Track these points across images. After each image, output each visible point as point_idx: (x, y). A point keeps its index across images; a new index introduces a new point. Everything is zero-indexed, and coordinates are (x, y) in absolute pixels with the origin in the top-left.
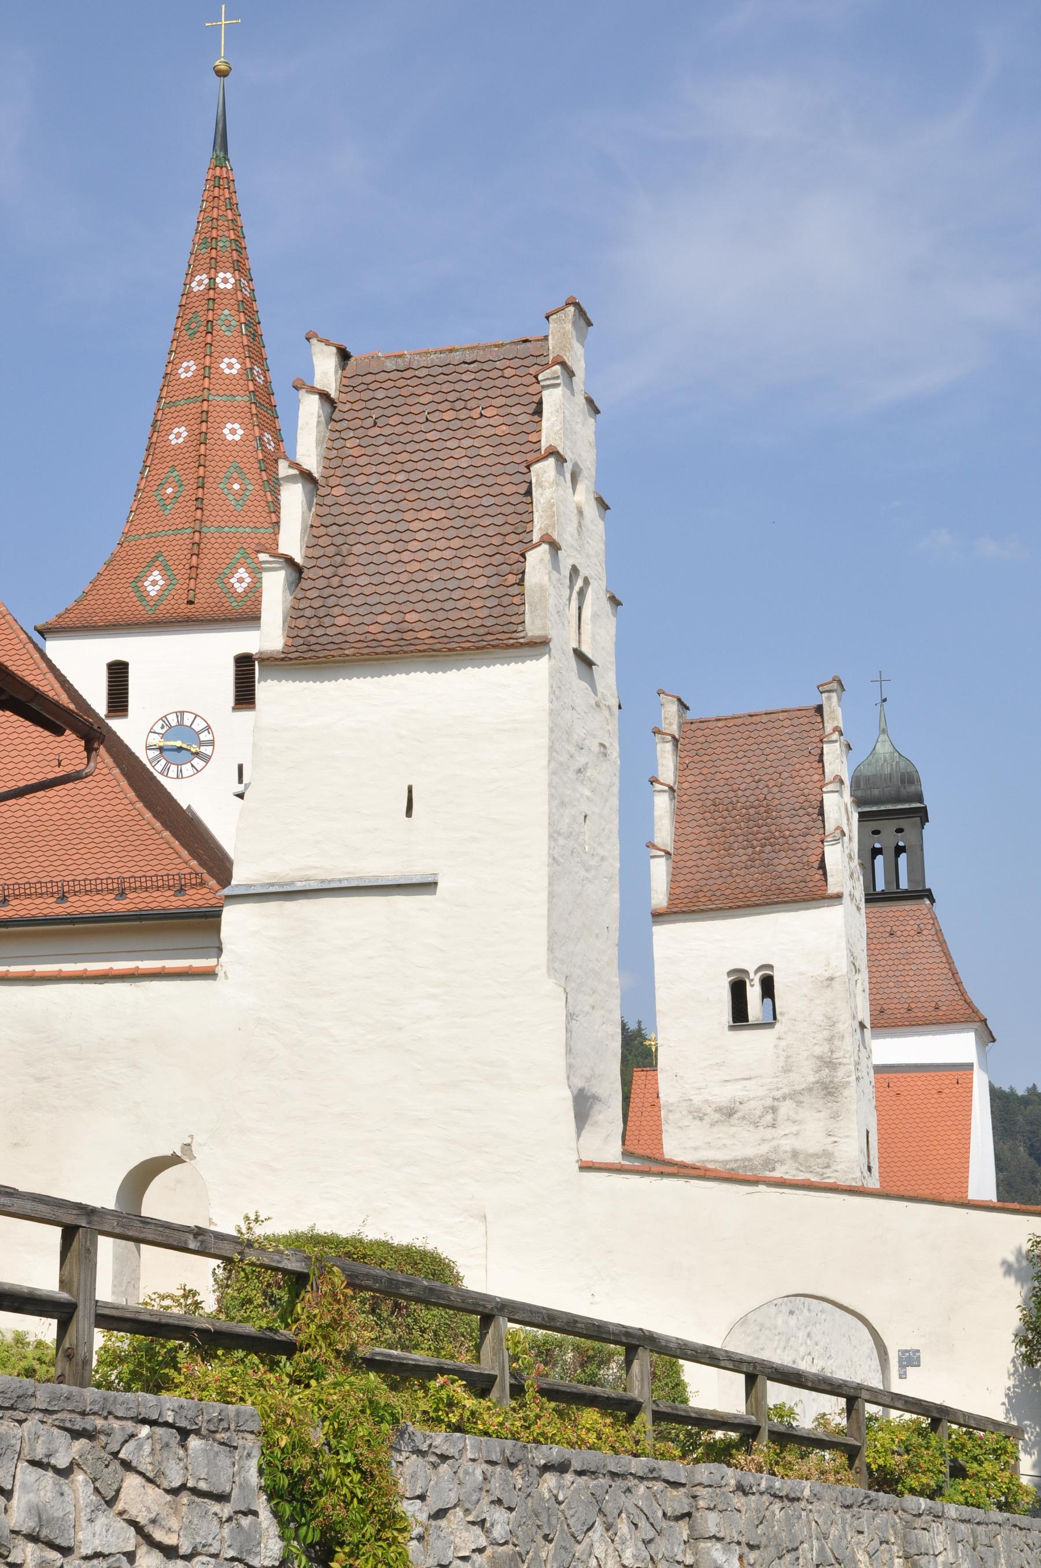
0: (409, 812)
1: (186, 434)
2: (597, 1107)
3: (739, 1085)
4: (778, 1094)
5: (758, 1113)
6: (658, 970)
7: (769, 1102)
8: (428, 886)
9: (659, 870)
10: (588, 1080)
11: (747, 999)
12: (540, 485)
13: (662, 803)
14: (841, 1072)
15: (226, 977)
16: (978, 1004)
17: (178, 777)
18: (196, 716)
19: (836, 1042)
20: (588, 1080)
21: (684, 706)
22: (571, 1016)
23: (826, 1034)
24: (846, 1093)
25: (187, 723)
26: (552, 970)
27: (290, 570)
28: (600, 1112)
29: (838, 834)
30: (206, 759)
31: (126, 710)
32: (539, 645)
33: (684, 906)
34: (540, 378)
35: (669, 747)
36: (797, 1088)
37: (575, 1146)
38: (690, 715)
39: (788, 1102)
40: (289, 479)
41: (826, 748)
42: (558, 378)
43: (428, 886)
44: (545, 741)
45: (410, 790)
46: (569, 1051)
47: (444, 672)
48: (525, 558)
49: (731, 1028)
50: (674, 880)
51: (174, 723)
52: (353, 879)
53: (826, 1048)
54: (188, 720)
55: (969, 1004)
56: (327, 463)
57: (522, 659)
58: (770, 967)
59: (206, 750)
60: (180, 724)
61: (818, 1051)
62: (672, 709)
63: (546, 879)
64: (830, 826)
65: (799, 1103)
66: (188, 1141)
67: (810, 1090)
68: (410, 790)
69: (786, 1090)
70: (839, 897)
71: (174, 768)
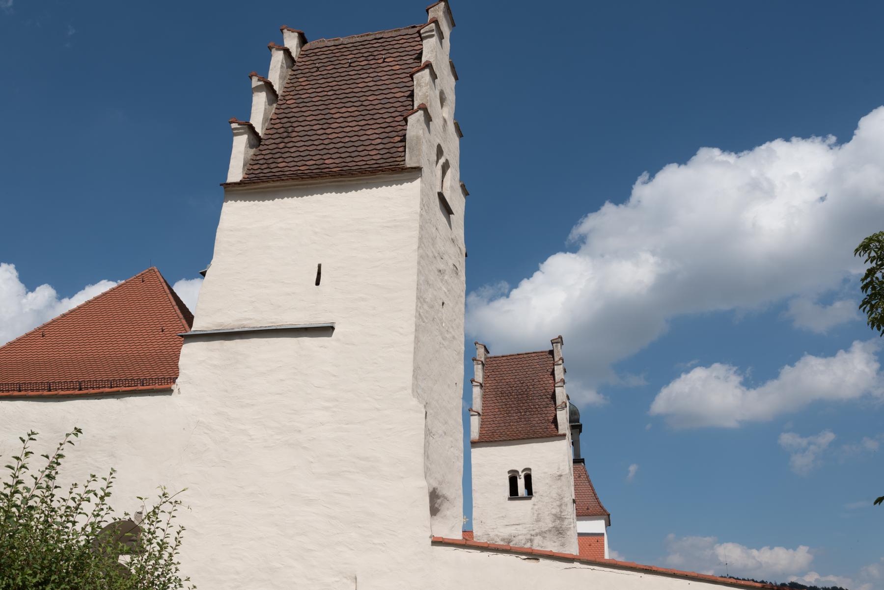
0: (318, 283)
2: (446, 505)
3: (514, 527)
4: (533, 533)
5: (523, 542)
6: (473, 469)
7: (529, 537)
8: (327, 330)
9: (475, 421)
10: (440, 483)
11: (520, 486)
12: (419, 85)
13: (477, 391)
14: (566, 523)
15: (179, 392)
16: (606, 507)
19: (563, 507)
20: (440, 483)
21: (487, 351)
22: (428, 432)
23: (558, 503)
24: (568, 533)
26: (416, 390)
27: (252, 137)
28: (448, 509)
29: (564, 405)
32: (416, 171)
33: (487, 439)
34: (422, 31)
35: (480, 366)
36: (543, 530)
37: (429, 525)
38: (489, 355)
39: (539, 537)
40: (258, 89)
41: (556, 367)
42: (432, 31)
43: (327, 330)
44: (416, 233)
45: (320, 266)
46: (427, 456)
47: (346, 192)
48: (406, 121)
49: (510, 499)
50: (482, 427)
53: (558, 510)
55: (602, 507)
56: (286, 90)
57: (400, 182)
58: (530, 469)
61: (554, 511)
62: (481, 351)
63: (414, 326)
64: (559, 402)
65: (544, 538)
66: (140, 510)
67: (550, 531)
68: (320, 266)
69: (537, 531)
70: (564, 435)
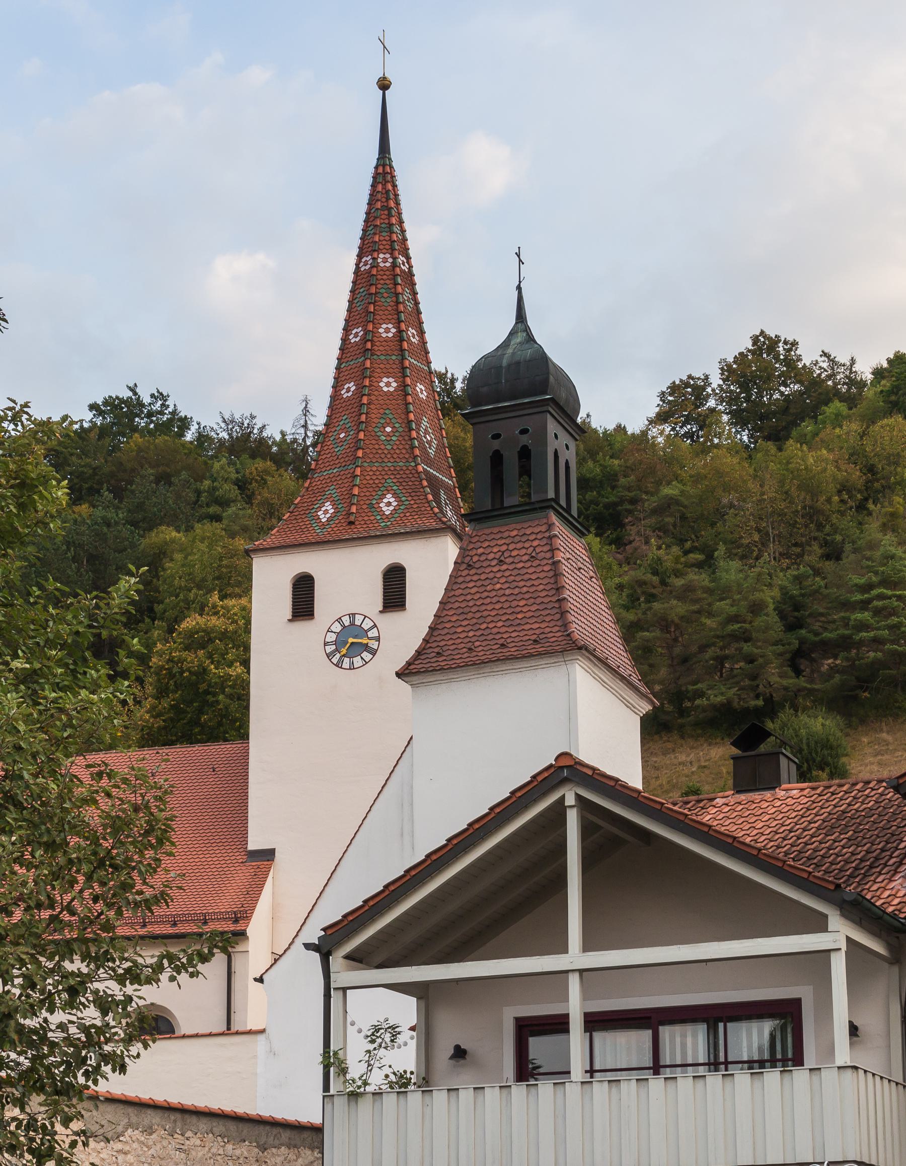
1: (354, 388)
17: (350, 669)
18: (365, 617)
25: (358, 623)
30: (374, 652)
31: (313, 615)
45: (411, 738)
51: (347, 623)
52: (622, 700)
54: (358, 620)
59: (374, 644)
60: (352, 624)
68: (411, 738)
71: (347, 660)
